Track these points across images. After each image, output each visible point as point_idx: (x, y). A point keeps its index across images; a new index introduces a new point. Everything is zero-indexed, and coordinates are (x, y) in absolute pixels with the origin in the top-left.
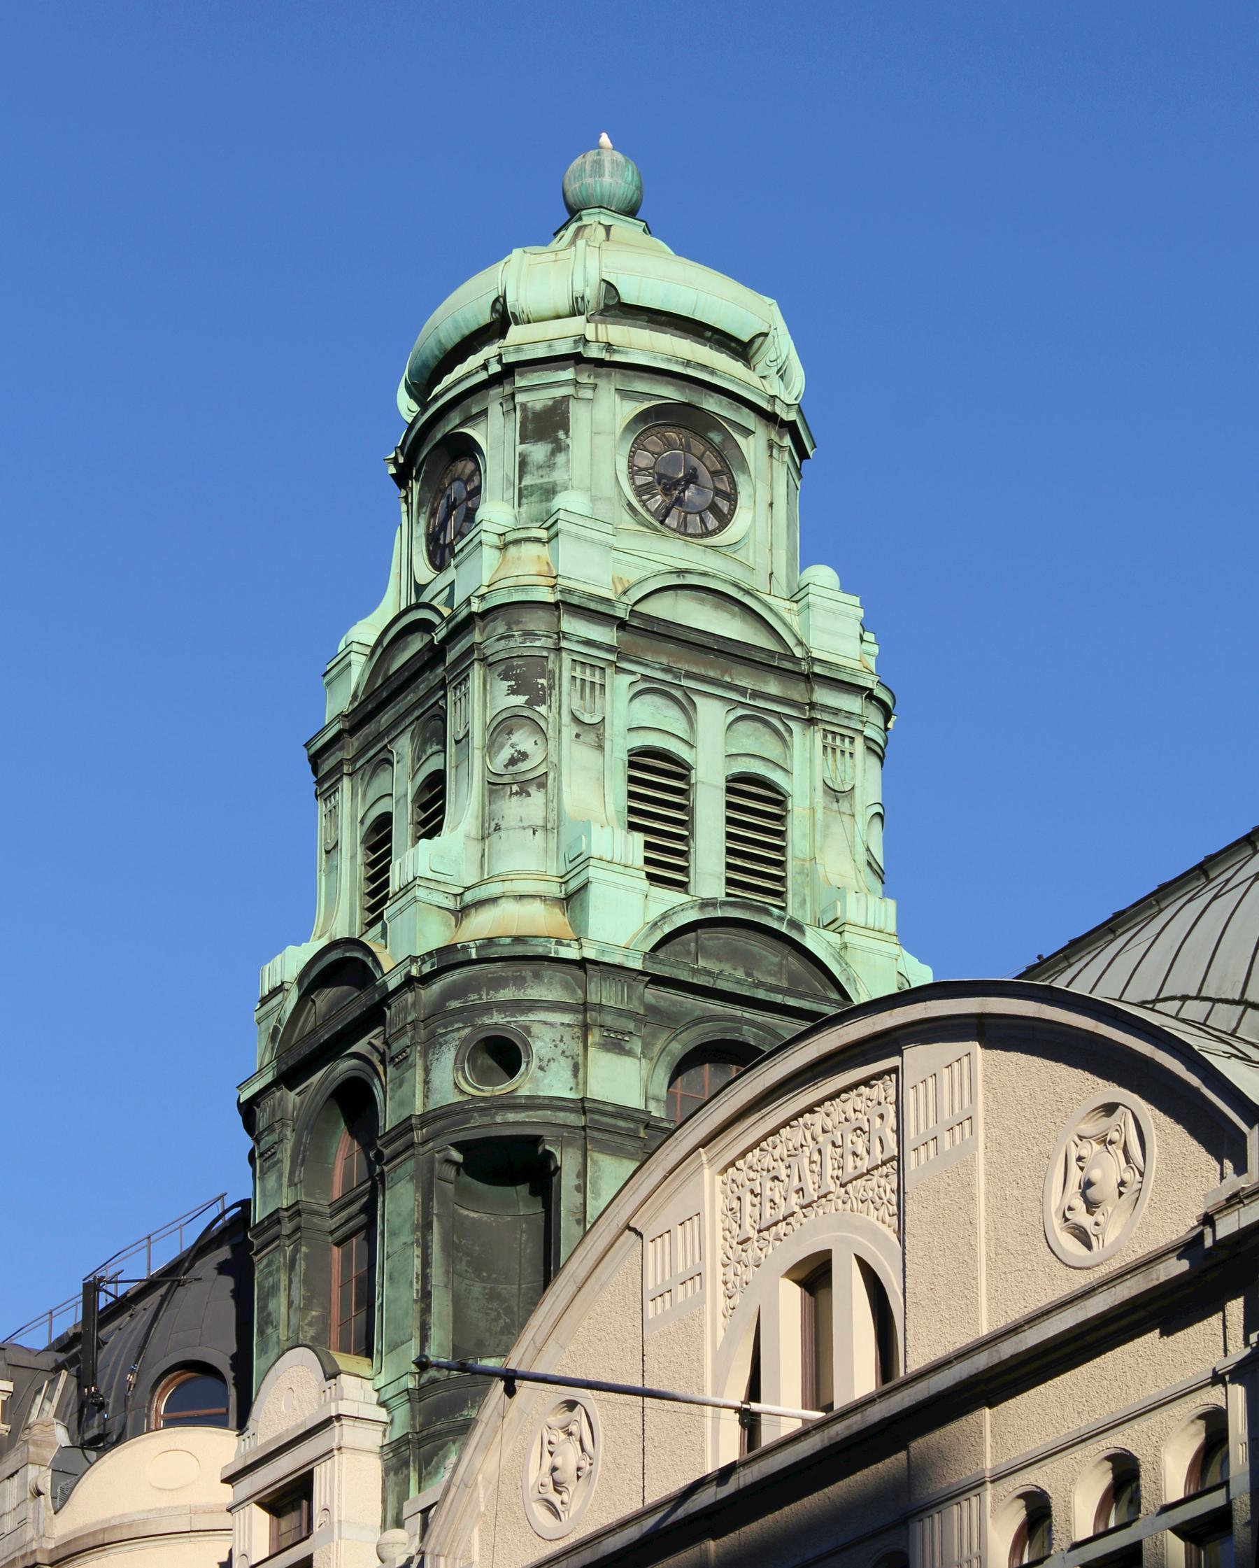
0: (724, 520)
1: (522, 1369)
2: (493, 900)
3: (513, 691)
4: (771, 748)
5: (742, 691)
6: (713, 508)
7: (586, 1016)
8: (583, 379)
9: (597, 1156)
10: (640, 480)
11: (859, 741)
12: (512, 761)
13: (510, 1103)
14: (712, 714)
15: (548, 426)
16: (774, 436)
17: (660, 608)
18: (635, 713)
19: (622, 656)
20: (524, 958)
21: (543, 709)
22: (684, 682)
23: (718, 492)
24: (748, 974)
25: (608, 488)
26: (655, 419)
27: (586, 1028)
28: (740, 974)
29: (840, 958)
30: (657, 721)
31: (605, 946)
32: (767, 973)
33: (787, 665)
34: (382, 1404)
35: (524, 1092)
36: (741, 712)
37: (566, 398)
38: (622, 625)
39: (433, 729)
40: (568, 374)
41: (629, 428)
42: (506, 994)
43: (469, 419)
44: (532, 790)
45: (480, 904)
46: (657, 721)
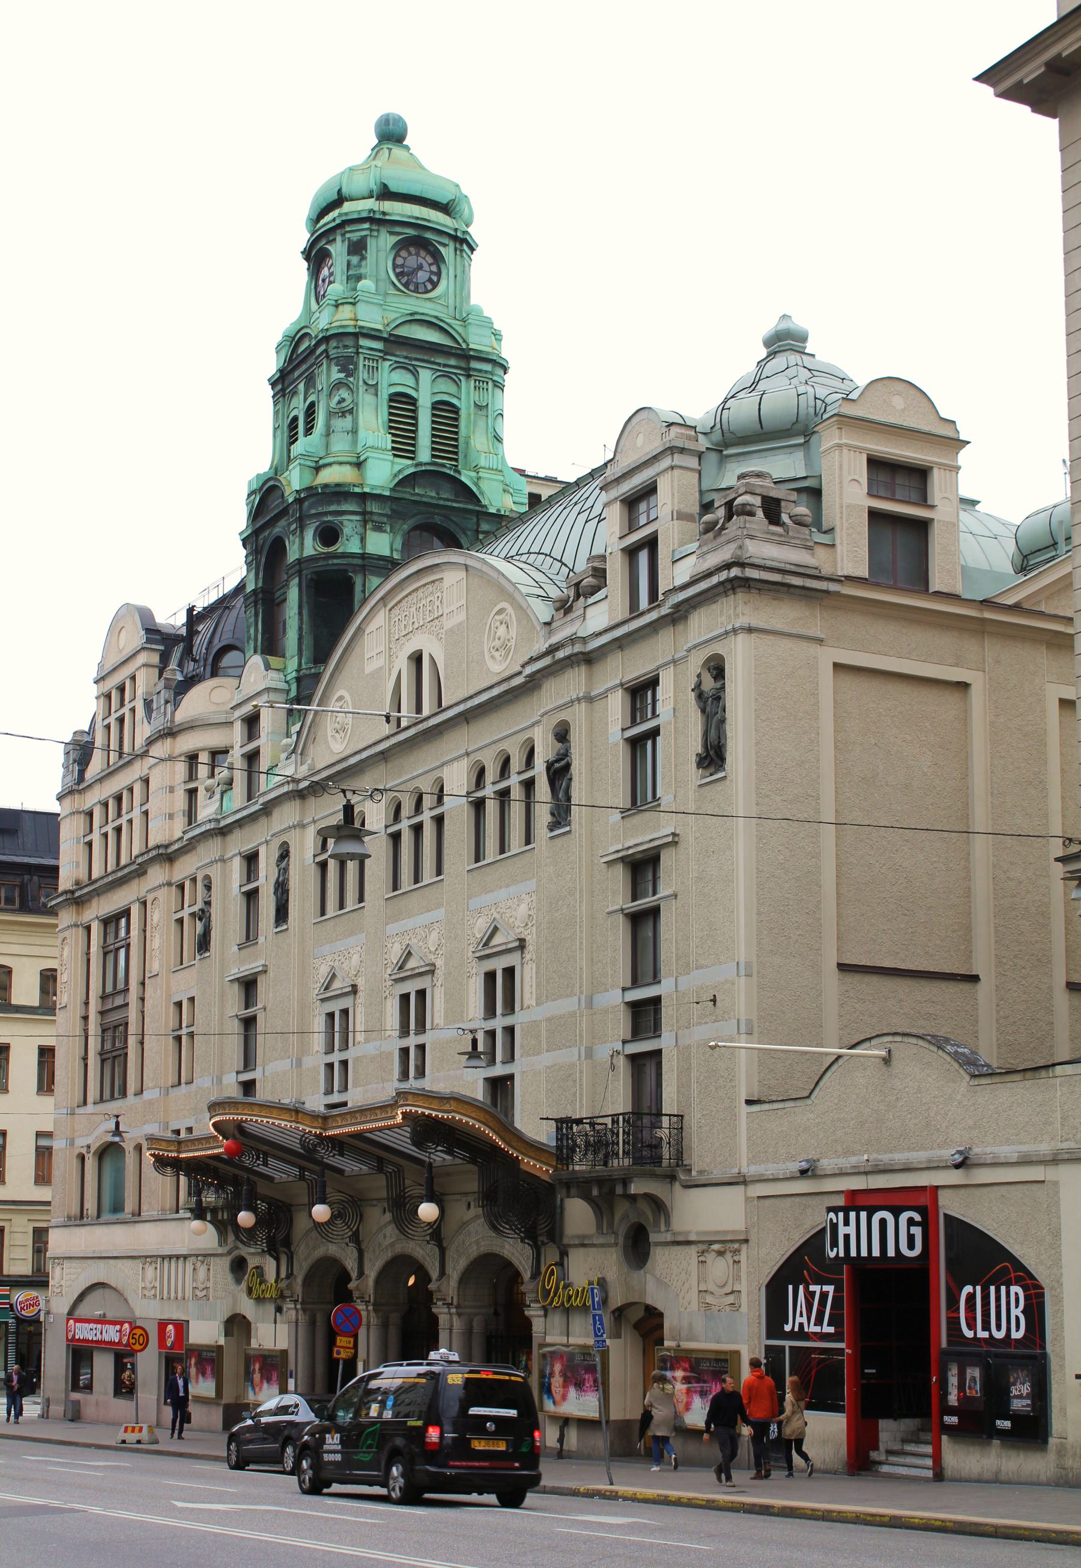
0: (435, 285)
1: (697, 489)
2: (330, 464)
3: (340, 371)
4: (452, 389)
5: (439, 364)
6: (430, 280)
7: (366, 517)
8: (374, 227)
9: (370, 577)
10: (398, 270)
11: (490, 384)
12: (339, 402)
13: (335, 555)
14: (425, 375)
15: (358, 248)
16: (458, 246)
17: (403, 332)
18: (392, 378)
19: (386, 354)
20: (338, 493)
21: (351, 379)
22: (413, 363)
23: (432, 272)
24: (438, 494)
25: (383, 275)
26: (404, 245)
27: (365, 522)
28: (433, 494)
29: (476, 485)
30: (401, 381)
31: (373, 487)
32: (445, 496)
33: (459, 352)
34: (287, 682)
35: (340, 551)
36: (439, 374)
37: (366, 236)
38: (384, 340)
39: (310, 382)
40: (367, 226)
41: (393, 248)
42: (333, 508)
43: (329, 242)
44: (347, 415)
45: (325, 466)
46: (401, 381)
